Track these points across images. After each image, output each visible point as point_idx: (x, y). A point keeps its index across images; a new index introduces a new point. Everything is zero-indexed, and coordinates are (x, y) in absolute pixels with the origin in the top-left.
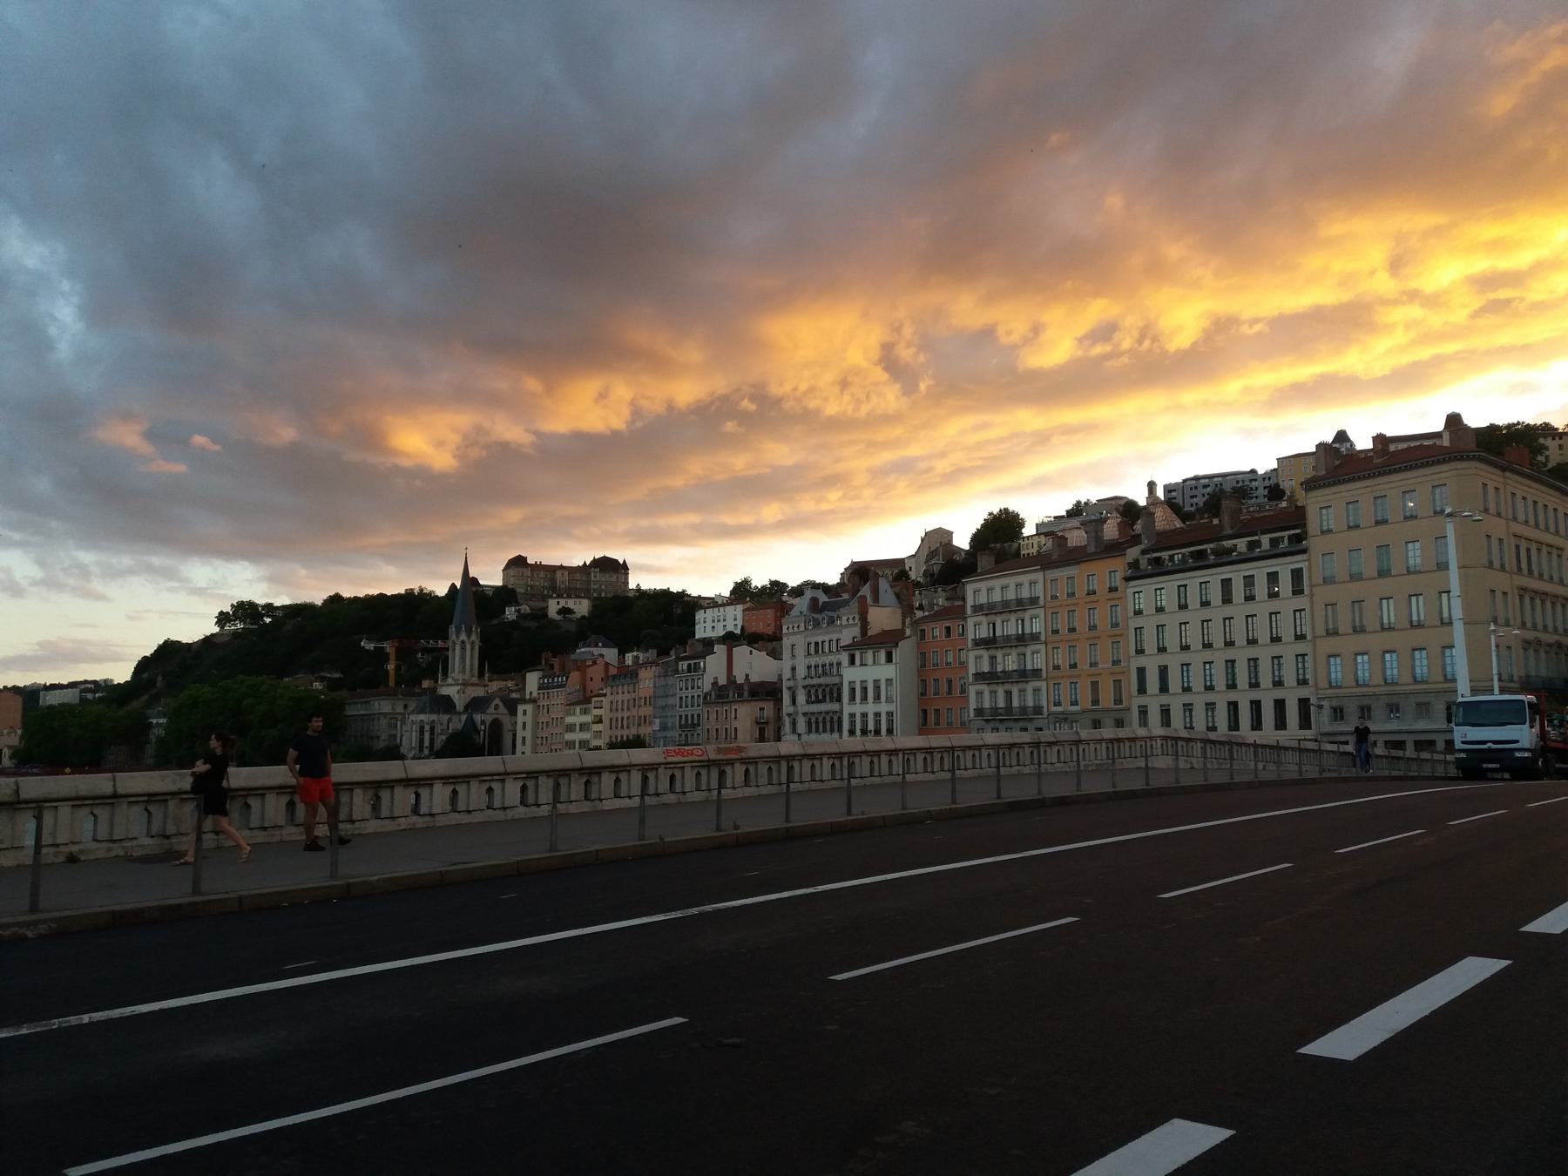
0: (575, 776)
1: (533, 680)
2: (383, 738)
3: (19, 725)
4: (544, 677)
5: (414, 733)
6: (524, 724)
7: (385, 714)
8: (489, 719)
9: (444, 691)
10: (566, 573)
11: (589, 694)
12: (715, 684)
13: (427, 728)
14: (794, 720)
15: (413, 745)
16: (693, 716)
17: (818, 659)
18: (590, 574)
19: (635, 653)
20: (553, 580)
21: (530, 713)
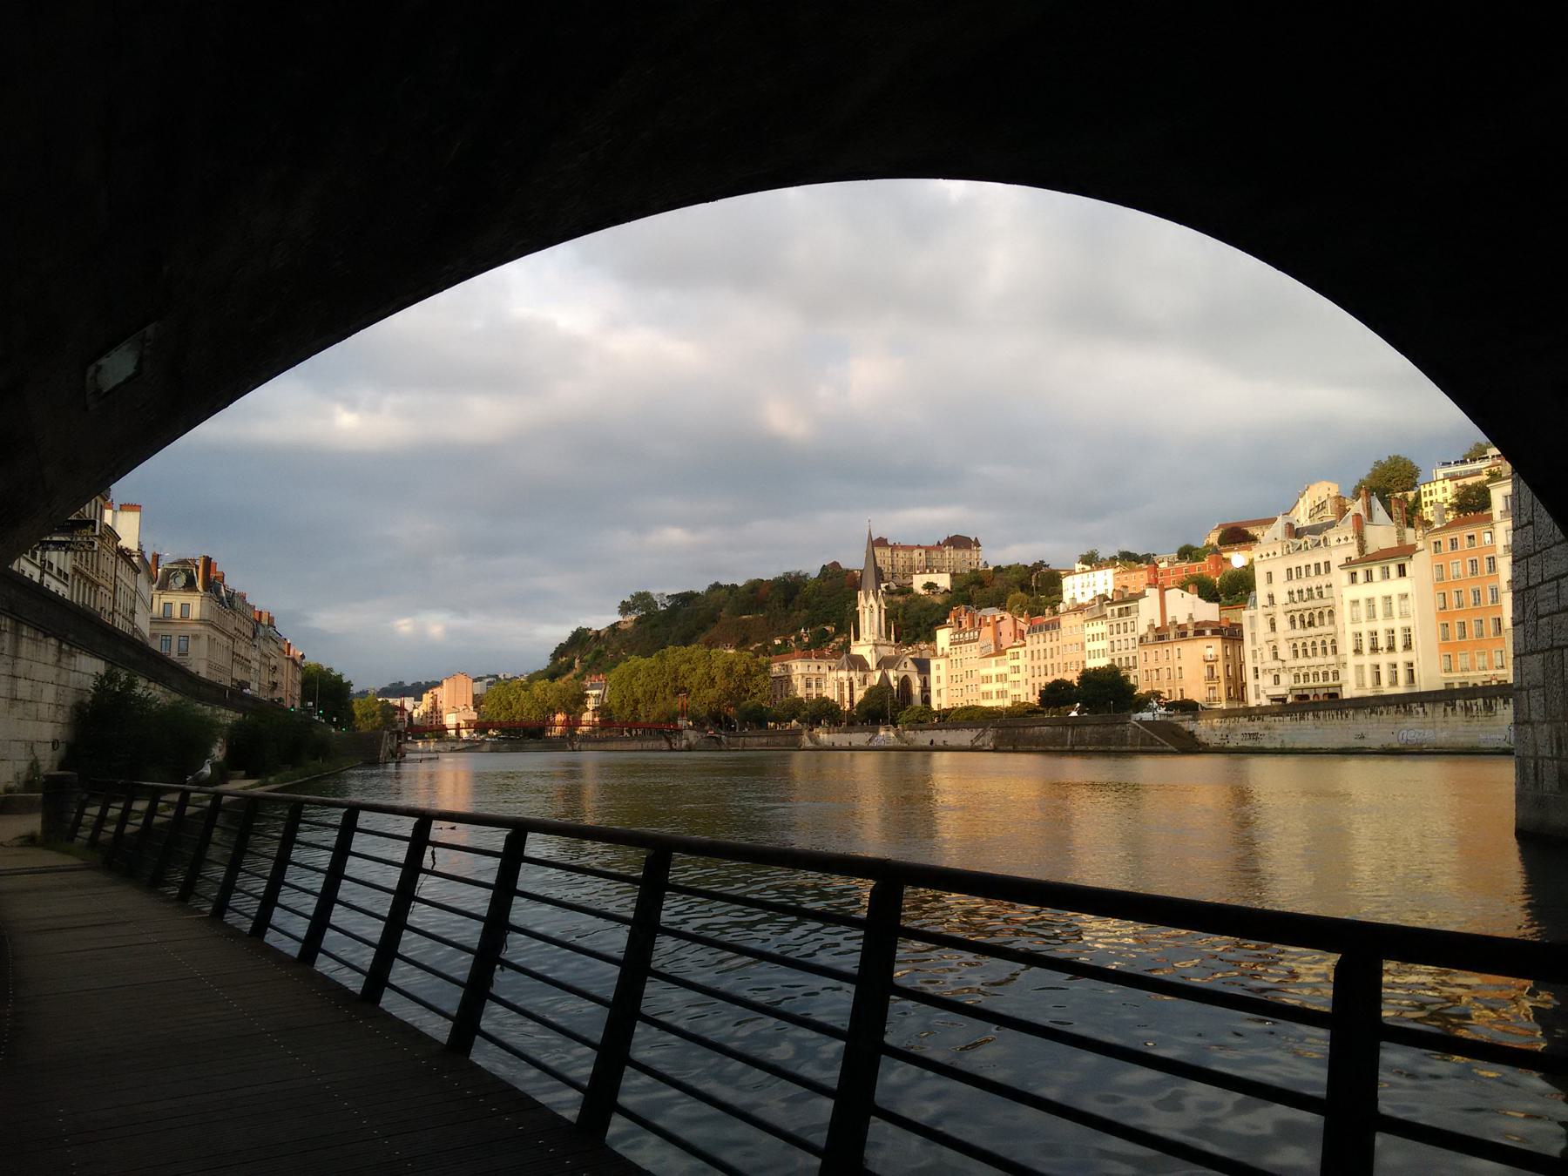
3: (471, 703)
4: (955, 633)
12: (1151, 626)
21: (943, 667)
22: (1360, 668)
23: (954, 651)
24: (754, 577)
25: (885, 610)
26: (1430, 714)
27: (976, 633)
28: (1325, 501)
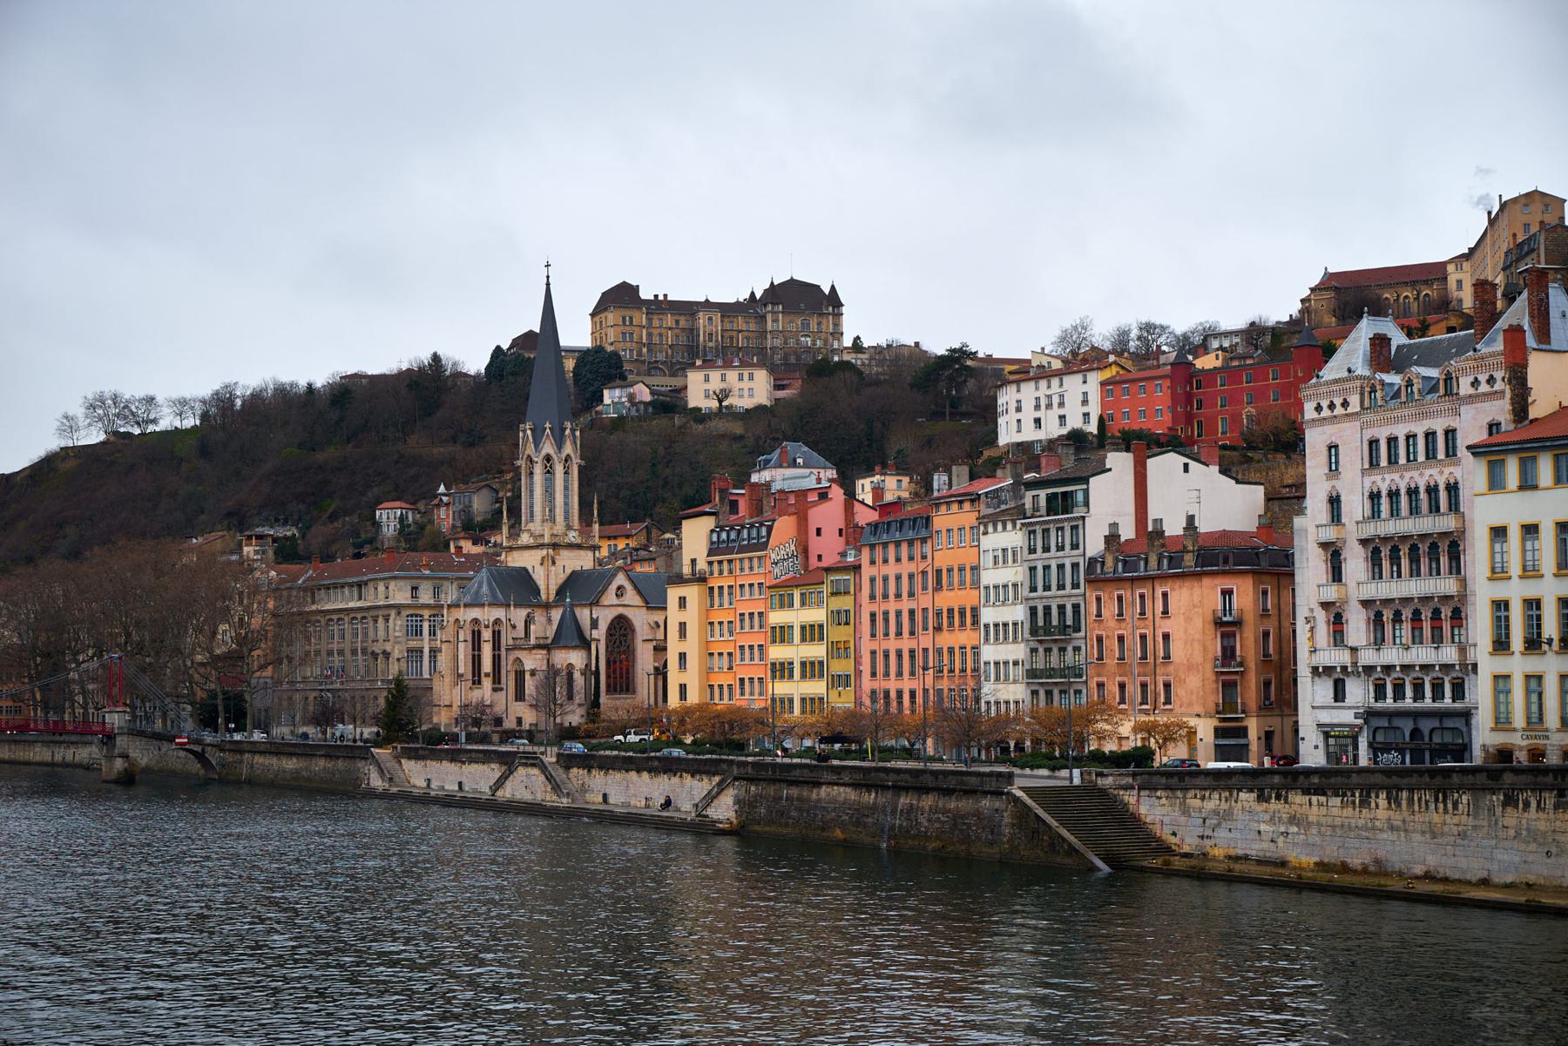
1: (695, 536)
2: (396, 654)
5: (461, 645)
6: (683, 626)
7: (399, 608)
8: (605, 616)
9: (516, 560)
10: (717, 317)
11: (814, 563)
12: (1112, 539)
13: (487, 635)
15: (461, 671)
16: (1062, 608)
17: (1396, 476)
18: (763, 317)
19: (877, 478)
20: (692, 332)
22: (1501, 680)
23: (716, 567)
24: (351, 370)
25: (580, 466)
27: (764, 531)
28: (1535, 234)
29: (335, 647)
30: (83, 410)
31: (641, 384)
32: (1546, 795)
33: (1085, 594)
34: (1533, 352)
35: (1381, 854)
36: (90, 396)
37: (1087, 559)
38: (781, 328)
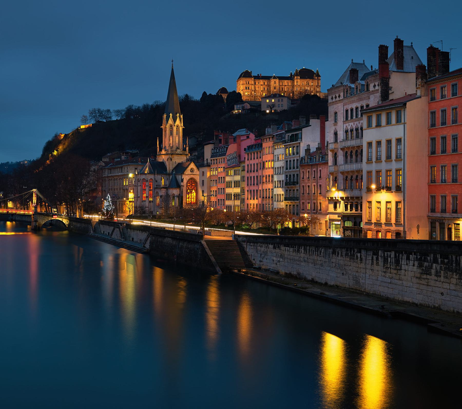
0: (323, 213)
14: (336, 178)
26: (251, 254)
29: (116, 187)
30: (89, 114)
31: (247, 103)
32: (343, 250)
33: (300, 171)
34: (393, 73)
35: (301, 271)
36: (91, 110)
37: (301, 158)
38: (299, 84)
